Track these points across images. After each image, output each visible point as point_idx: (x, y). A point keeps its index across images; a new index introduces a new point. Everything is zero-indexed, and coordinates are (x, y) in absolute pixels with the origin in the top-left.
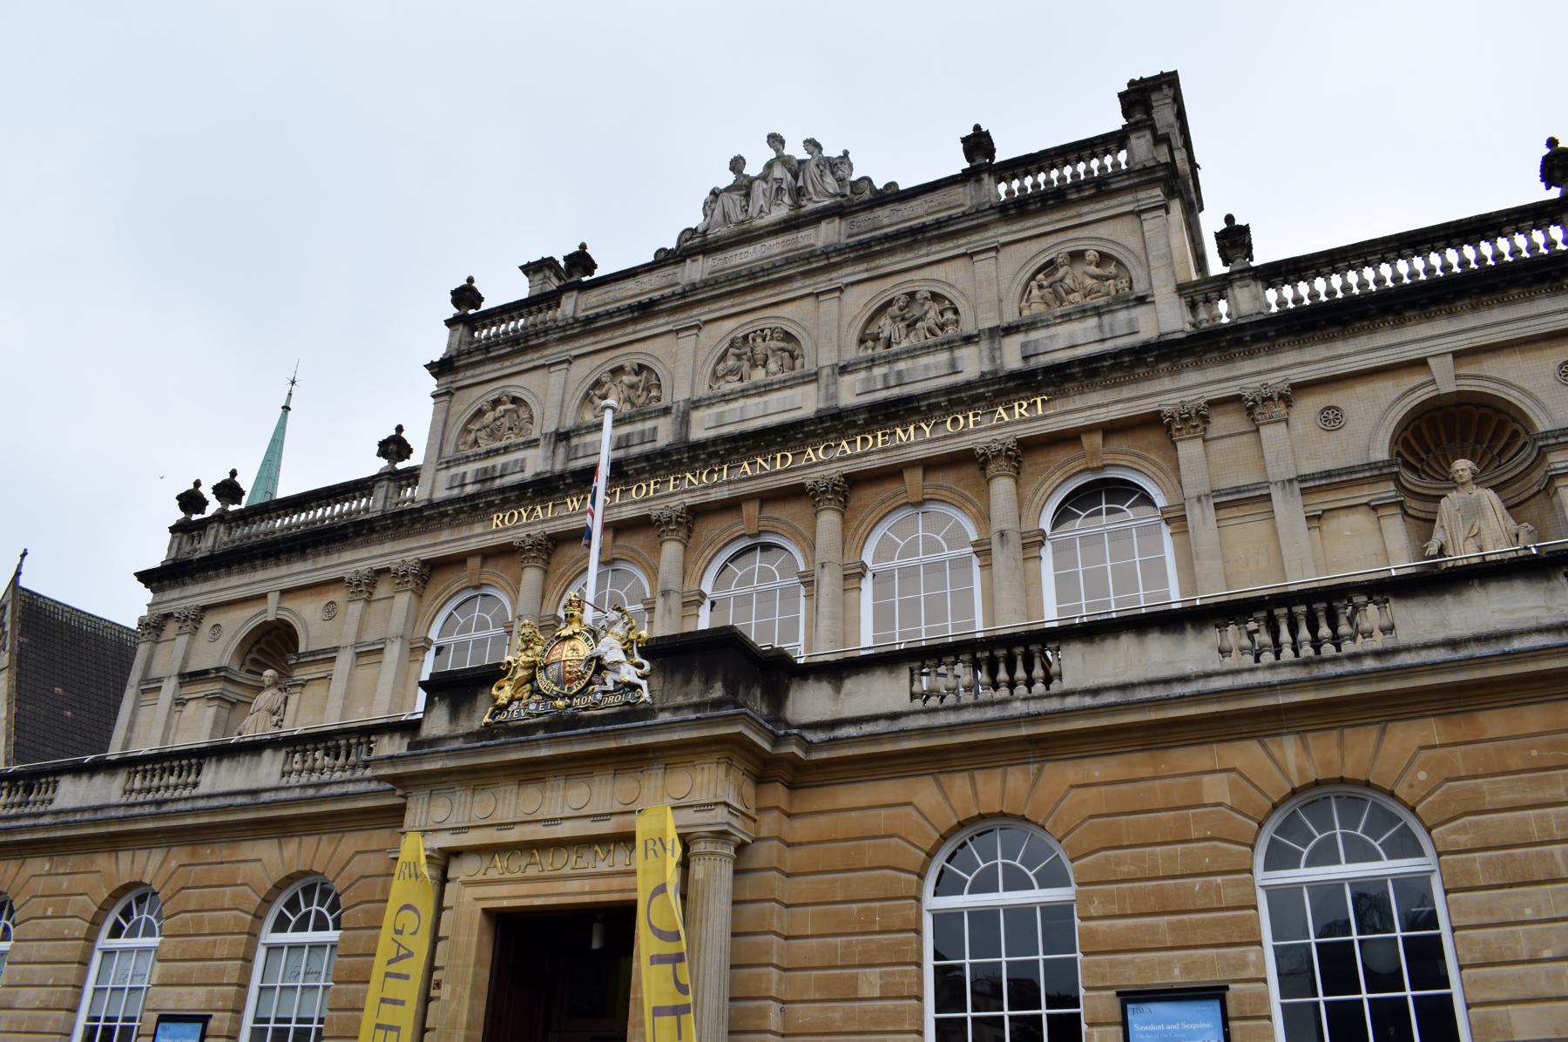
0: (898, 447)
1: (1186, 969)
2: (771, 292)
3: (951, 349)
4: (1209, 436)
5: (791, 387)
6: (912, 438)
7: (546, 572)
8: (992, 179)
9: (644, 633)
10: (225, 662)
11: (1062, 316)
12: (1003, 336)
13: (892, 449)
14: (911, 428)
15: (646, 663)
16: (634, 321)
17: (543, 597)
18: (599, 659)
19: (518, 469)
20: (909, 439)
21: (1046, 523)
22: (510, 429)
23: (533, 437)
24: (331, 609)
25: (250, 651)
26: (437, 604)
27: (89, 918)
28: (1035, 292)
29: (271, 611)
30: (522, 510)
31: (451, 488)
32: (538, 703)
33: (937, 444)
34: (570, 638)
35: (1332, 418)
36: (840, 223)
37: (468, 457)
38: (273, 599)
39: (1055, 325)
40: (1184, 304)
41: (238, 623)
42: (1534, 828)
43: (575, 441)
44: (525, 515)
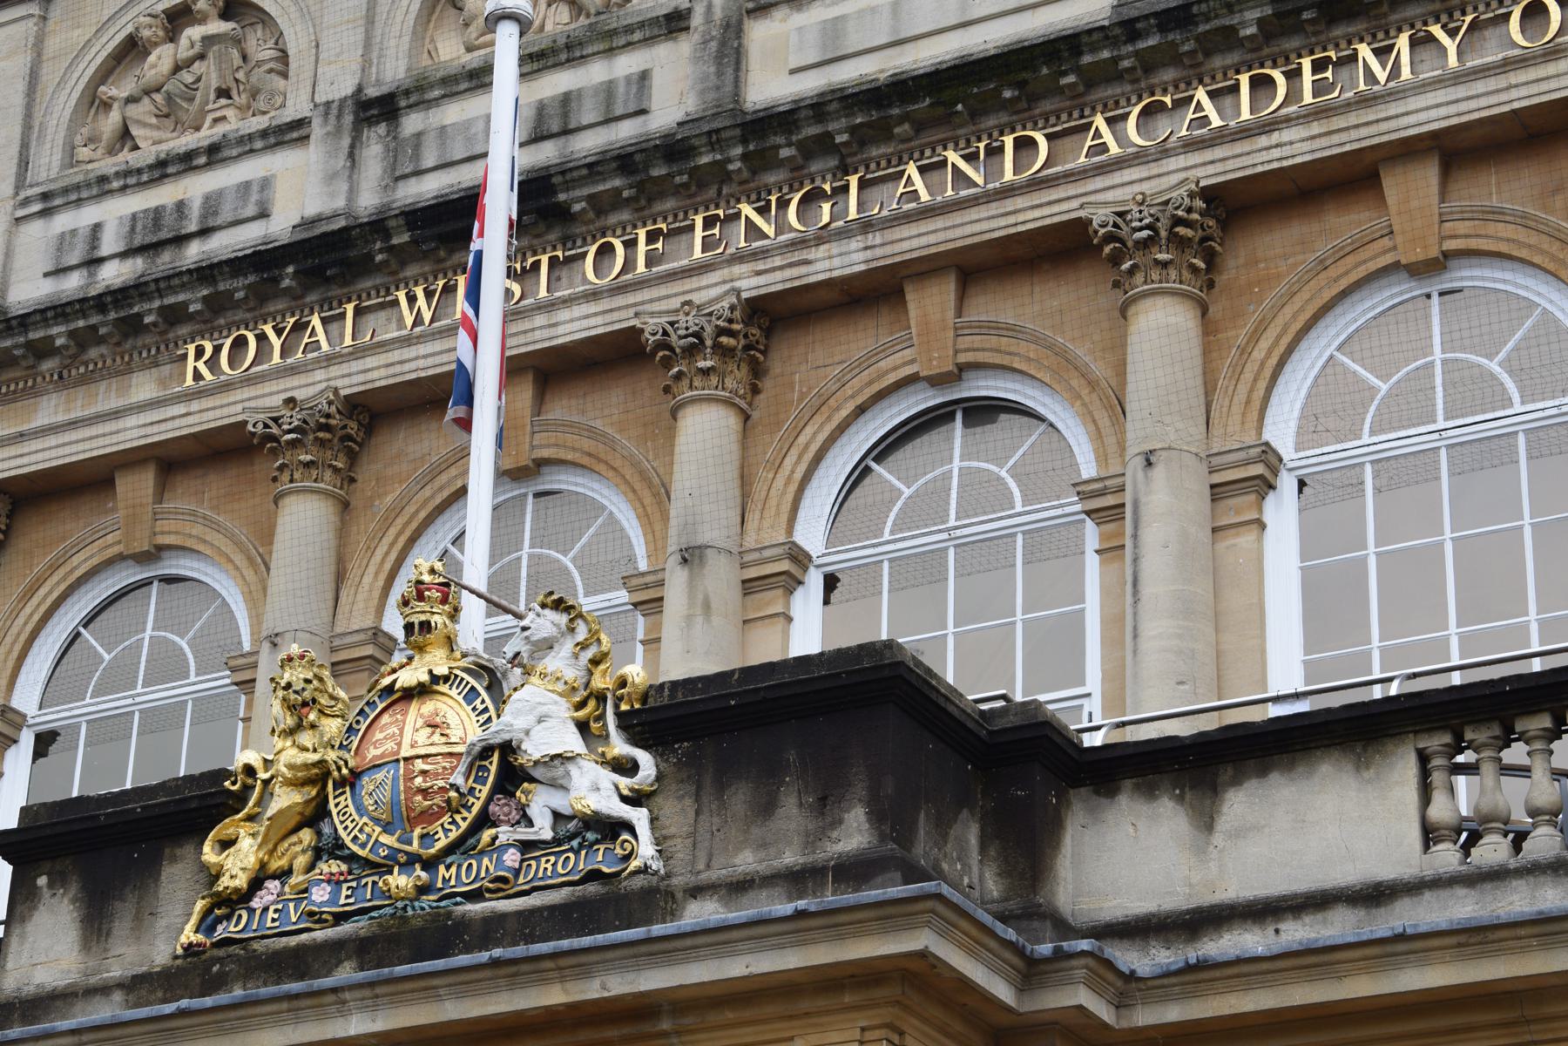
0: (1364, 101)
6: (1406, 73)
7: (345, 506)
9: (636, 672)
13: (1348, 107)
15: (645, 759)
17: (340, 577)
18: (508, 749)
19: (251, 210)
20: (1395, 73)
23: (289, 115)
30: (268, 329)
31: (59, 271)
32: (335, 882)
33: (1480, 87)
34: (421, 691)
43: (412, 123)
44: (276, 343)
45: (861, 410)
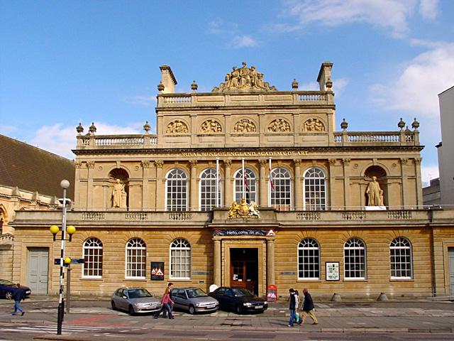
35: (356, 165)
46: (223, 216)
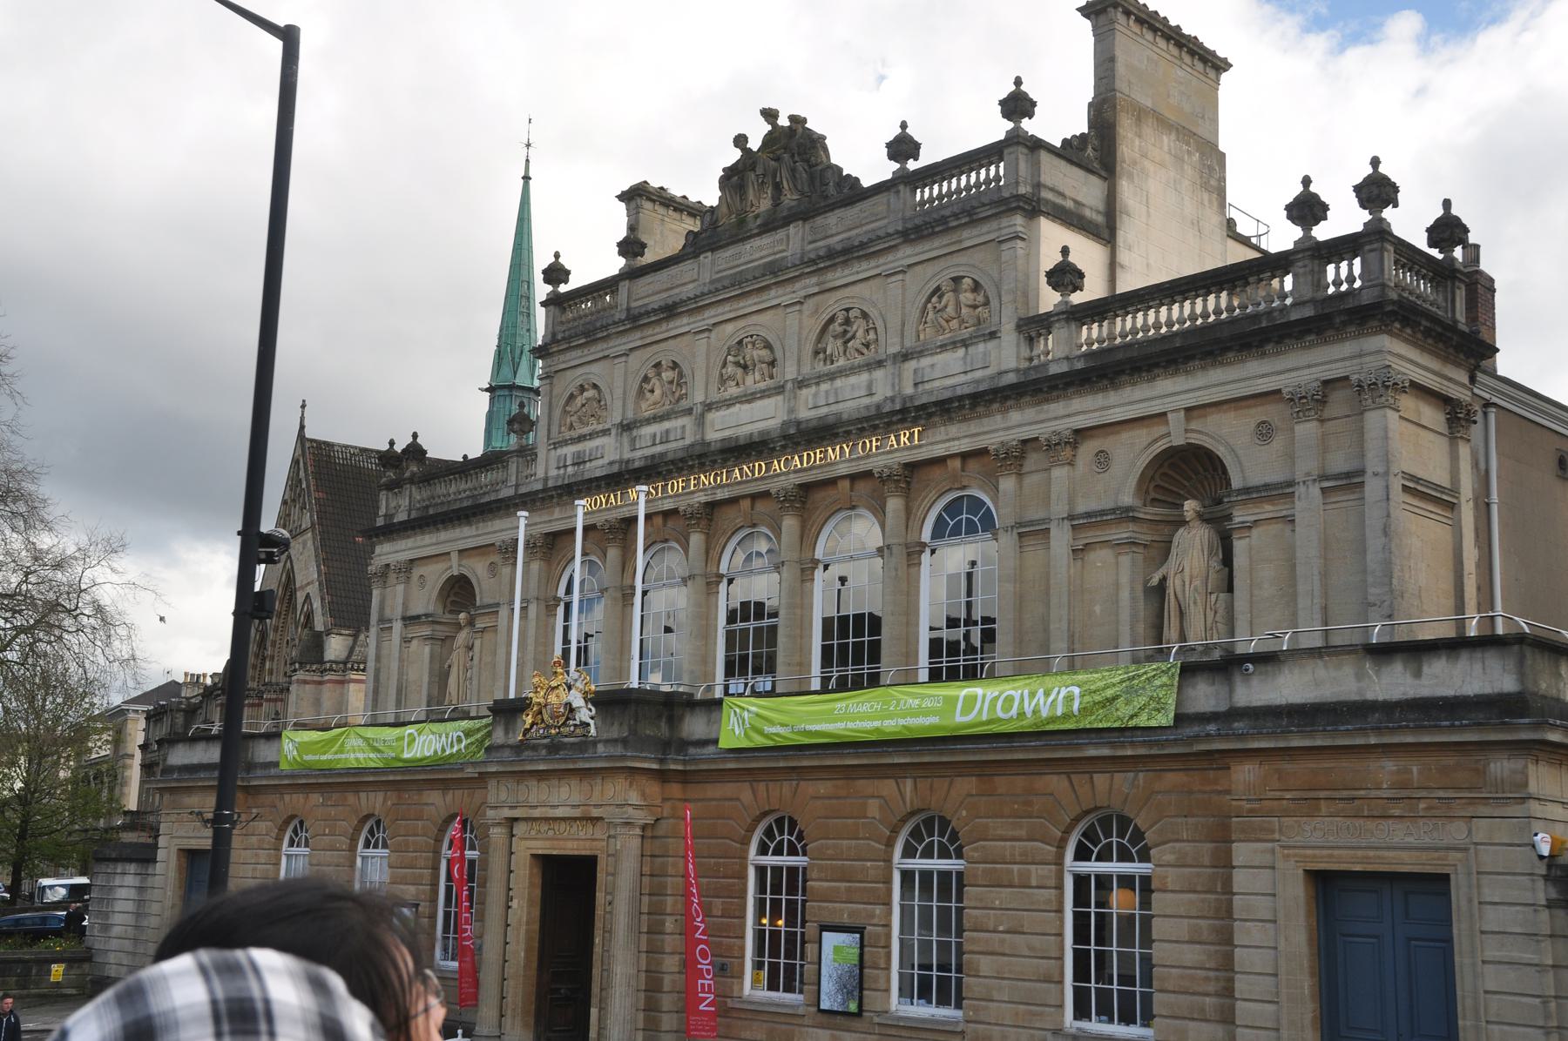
1: (850, 916)
2: (756, 300)
3: (869, 370)
4: (1025, 469)
5: (769, 396)
7: (624, 547)
8: (908, 189)
9: (593, 688)
10: (431, 609)
11: (941, 346)
12: (903, 361)
14: (838, 447)
15: (593, 709)
16: (667, 319)
18: (570, 704)
19: (599, 456)
21: (926, 536)
22: (592, 416)
23: (607, 427)
24: (1265, 432)
25: (449, 596)
26: (560, 568)
27: (349, 836)
28: (931, 315)
29: (455, 567)
31: (559, 468)
34: (557, 687)
36: (803, 226)
37: (566, 441)
38: (454, 556)
39: (937, 353)
40: (1022, 339)
41: (436, 575)
42: (1008, 853)
43: (635, 433)
45: (733, 534)
46: (511, 735)
